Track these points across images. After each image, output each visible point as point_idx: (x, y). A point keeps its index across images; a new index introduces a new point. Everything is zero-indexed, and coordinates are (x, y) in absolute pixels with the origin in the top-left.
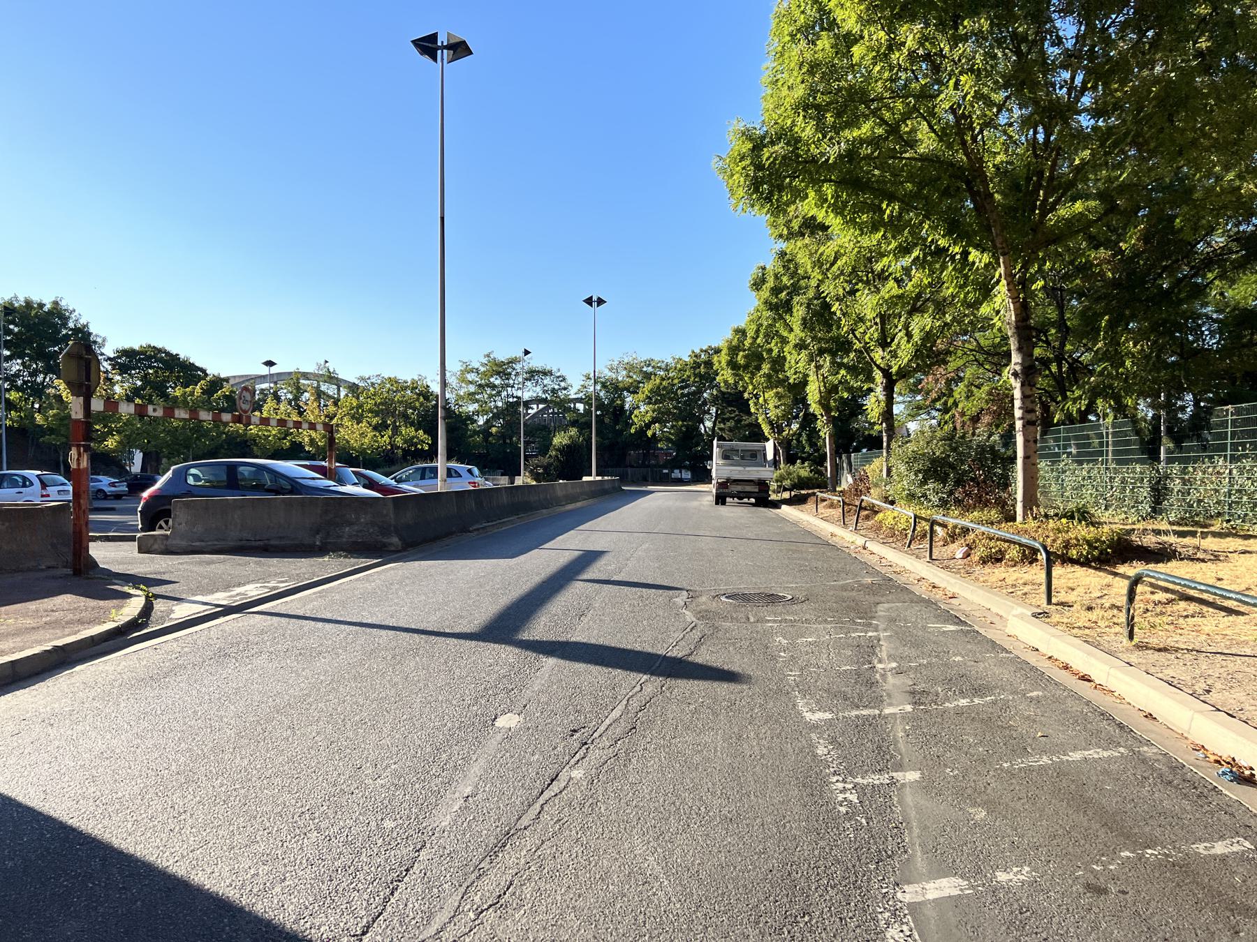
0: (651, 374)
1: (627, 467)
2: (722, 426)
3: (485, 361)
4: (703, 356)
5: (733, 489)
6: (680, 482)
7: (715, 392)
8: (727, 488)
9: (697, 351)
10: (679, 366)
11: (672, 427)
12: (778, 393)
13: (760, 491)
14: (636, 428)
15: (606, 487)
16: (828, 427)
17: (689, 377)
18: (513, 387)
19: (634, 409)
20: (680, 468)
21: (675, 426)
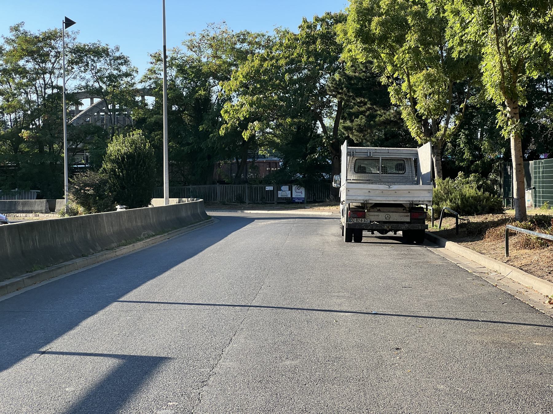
0: (247, 52)
1: (214, 183)
2: (348, 123)
3: (11, 35)
4: (318, 27)
5: (373, 219)
6: (290, 203)
7: (337, 76)
8: (364, 216)
9: (311, 20)
10: (285, 42)
11: (278, 126)
12: (429, 75)
13: (413, 220)
14: (227, 128)
15: (183, 214)
16: (513, 123)
17: (300, 55)
18: (51, 73)
19: (224, 101)
20: (290, 183)
21: (281, 125)
